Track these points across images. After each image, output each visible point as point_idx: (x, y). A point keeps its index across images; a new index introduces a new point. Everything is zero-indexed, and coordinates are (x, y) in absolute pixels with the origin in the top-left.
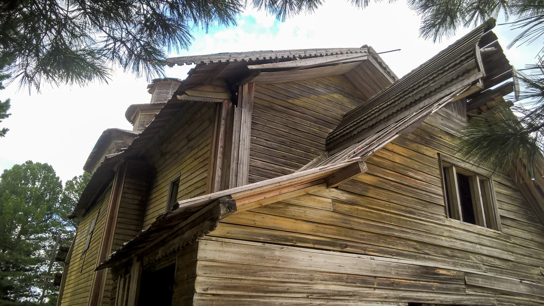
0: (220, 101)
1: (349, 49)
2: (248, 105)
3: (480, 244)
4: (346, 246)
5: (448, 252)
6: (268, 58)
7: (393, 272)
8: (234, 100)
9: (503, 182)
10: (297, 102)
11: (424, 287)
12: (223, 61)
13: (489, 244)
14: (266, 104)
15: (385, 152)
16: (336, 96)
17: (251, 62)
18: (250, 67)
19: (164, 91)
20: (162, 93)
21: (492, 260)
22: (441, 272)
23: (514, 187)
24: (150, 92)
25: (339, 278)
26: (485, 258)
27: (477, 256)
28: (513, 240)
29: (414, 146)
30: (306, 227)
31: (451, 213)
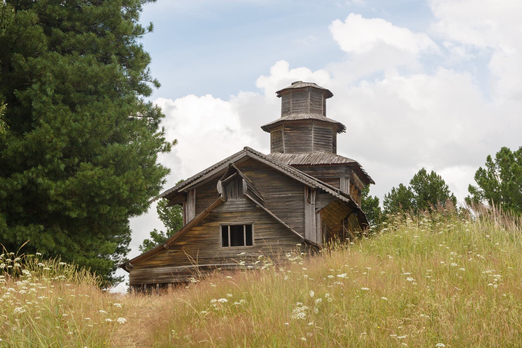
1: (233, 156)
9: (264, 222)
17: (180, 189)
18: (179, 191)
28: (263, 248)
29: (206, 224)
30: (160, 262)
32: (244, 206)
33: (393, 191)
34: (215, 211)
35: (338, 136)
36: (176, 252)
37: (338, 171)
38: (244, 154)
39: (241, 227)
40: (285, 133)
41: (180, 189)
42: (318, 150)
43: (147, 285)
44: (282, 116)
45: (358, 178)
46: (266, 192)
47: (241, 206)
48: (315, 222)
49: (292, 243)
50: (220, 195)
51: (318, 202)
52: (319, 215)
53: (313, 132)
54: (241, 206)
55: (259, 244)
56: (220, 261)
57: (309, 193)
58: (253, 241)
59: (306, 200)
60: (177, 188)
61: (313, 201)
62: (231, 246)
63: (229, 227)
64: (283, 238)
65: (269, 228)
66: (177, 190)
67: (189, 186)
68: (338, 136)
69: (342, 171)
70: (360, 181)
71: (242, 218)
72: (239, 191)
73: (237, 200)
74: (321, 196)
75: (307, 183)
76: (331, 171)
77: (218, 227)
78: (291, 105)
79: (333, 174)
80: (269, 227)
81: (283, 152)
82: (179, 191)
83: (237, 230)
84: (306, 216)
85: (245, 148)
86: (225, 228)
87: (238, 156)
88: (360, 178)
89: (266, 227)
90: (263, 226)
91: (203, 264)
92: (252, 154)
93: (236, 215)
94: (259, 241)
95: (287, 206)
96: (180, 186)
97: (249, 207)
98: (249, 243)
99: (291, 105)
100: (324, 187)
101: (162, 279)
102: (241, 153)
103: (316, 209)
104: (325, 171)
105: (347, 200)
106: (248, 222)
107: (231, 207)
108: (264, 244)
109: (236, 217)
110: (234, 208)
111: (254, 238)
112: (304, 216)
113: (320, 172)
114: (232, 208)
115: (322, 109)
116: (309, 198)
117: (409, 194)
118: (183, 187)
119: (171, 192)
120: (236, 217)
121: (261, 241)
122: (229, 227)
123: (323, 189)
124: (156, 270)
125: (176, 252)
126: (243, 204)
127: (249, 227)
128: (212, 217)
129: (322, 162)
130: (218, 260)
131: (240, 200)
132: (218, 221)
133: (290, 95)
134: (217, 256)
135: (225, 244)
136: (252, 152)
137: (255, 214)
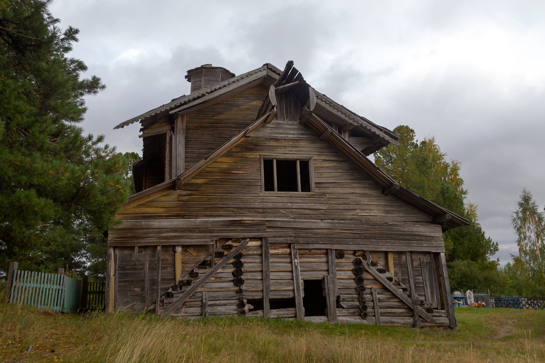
0: (165, 132)
1: (249, 73)
2: (182, 131)
3: (291, 203)
4: (185, 216)
5: (261, 211)
6: (182, 102)
7: (209, 225)
8: (173, 129)
9: (327, 159)
10: (221, 117)
11: (233, 230)
12: (153, 114)
13: (300, 202)
14: (196, 125)
15: (215, 164)
16: (254, 103)
17: (172, 109)
18: (171, 112)
19: (198, 80)
20: (196, 82)
21: (302, 211)
22: (246, 222)
23: (340, 159)
24: (189, 81)
25: (175, 230)
26: (295, 210)
27: (287, 210)
28: (328, 196)
29: (239, 154)
30: (162, 210)
31: (269, 187)
32: (295, 132)
34: (204, 151)
36: (190, 195)
38: (264, 73)
39: (293, 163)
41: (172, 109)
47: (292, 132)
49: (368, 192)
50: (273, 107)
54: (292, 132)
58: (313, 185)
60: (168, 108)
62: (278, 191)
63: (275, 161)
65: (335, 168)
66: (167, 111)
67: (182, 108)
71: (294, 149)
72: (286, 109)
73: (285, 122)
78: (203, 83)
80: (335, 167)
86: (268, 163)
87: (255, 75)
90: (327, 164)
91: (235, 216)
92: (274, 73)
93: (286, 144)
94: (321, 185)
96: (173, 106)
97: (302, 134)
98: (306, 187)
99: (203, 83)
102: (259, 70)
107: (276, 131)
109: (285, 147)
114: (278, 133)
118: (177, 107)
119: (158, 112)
120: (285, 147)
122: (275, 161)
123: (368, 128)
124: (156, 223)
125: (190, 195)
126: (294, 129)
127: (305, 164)
130: (260, 213)
131: (290, 122)
134: (257, 205)
135: (269, 187)
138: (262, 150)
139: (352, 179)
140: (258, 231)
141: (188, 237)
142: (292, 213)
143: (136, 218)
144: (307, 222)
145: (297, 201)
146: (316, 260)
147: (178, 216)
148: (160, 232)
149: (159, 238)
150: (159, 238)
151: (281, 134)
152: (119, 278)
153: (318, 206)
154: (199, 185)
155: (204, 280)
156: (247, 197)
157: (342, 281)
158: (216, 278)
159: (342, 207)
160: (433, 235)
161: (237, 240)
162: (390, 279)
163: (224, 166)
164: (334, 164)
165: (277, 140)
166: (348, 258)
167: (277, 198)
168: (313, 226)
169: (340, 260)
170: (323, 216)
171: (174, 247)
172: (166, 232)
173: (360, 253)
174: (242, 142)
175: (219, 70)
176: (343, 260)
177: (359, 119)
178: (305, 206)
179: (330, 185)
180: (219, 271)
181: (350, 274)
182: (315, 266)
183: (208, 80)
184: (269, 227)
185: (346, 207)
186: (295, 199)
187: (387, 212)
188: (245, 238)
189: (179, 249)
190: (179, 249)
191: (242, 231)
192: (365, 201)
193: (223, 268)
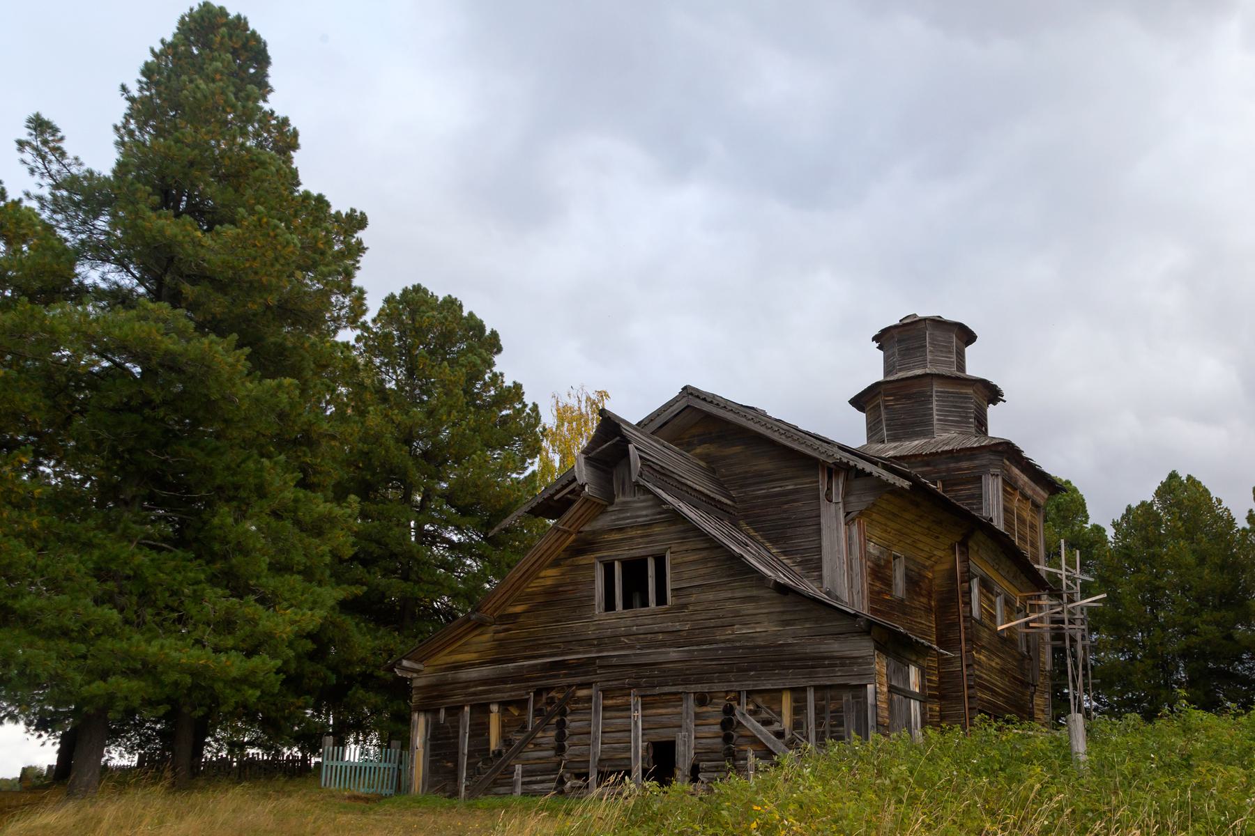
18: (556, 498)
25: (484, 682)
29: (569, 561)
30: (474, 655)
33: (191, 10)
35: (992, 410)
37: (977, 462)
39: (642, 562)
40: (886, 407)
42: (946, 431)
43: (447, 709)
44: (885, 375)
45: (1026, 479)
46: (742, 486)
48: (843, 544)
49: (755, 592)
51: (852, 499)
52: (855, 529)
53: (935, 398)
54: (644, 513)
55: (684, 600)
56: (598, 645)
57: (830, 478)
59: (822, 495)
61: (837, 495)
64: (735, 581)
68: (992, 410)
69: (984, 462)
70: (1033, 485)
71: (646, 540)
74: (857, 484)
75: (815, 454)
76: (965, 464)
77: (591, 567)
79: (968, 469)
81: (883, 442)
82: (556, 498)
83: (635, 570)
84: (825, 532)
85: (685, 388)
88: (1030, 478)
89: (696, 557)
91: (562, 655)
95: (785, 512)
98: (661, 599)
100: (847, 455)
101: (474, 694)
102: (675, 400)
103: (848, 514)
104: (952, 465)
105: (906, 484)
106: (657, 548)
108: (693, 599)
109: (632, 538)
110: (628, 518)
111: (669, 586)
112: (819, 531)
113: (943, 467)
115: (954, 359)
116: (830, 489)
117: (1158, 522)
121: (686, 592)
122: (616, 563)
123: (852, 463)
128: (584, 546)
129: (946, 448)
131: (642, 498)
132: (593, 551)
133: (900, 339)
135: (610, 605)
136: (698, 397)
137: (673, 528)
138: (598, 550)
139: (732, 575)
140: (586, 673)
141: (498, 691)
142: (638, 640)
143: (446, 669)
144: (650, 654)
145: (647, 621)
146: (669, 710)
147: (493, 662)
148: (467, 687)
149: (467, 695)
150: (467, 695)
151: (628, 518)
152: (431, 750)
153: (678, 626)
154: (517, 615)
155: (519, 747)
156: (577, 624)
157: (704, 741)
158: (535, 745)
159: (712, 623)
160: (856, 654)
161: (561, 689)
162: (780, 735)
163: (549, 582)
164: (704, 554)
165: (620, 530)
166: (717, 704)
167: (622, 619)
168: (661, 659)
169: (704, 709)
170: (676, 640)
171: (487, 705)
172: (476, 686)
173: (733, 695)
174: (574, 541)
175: (922, 325)
176: (708, 709)
177: (836, 449)
178: (656, 628)
179: (694, 591)
180: (539, 735)
181: (717, 728)
182: (665, 720)
183: (908, 349)
184: (601, 667)
185: (719, 622)
186: (649, 616)
187: (786, 623)
188: (570, 686)
189: (494, 708)
190: (494, 708)
191: (566, 675)
192: (749, 608)
193: (544, 731)
